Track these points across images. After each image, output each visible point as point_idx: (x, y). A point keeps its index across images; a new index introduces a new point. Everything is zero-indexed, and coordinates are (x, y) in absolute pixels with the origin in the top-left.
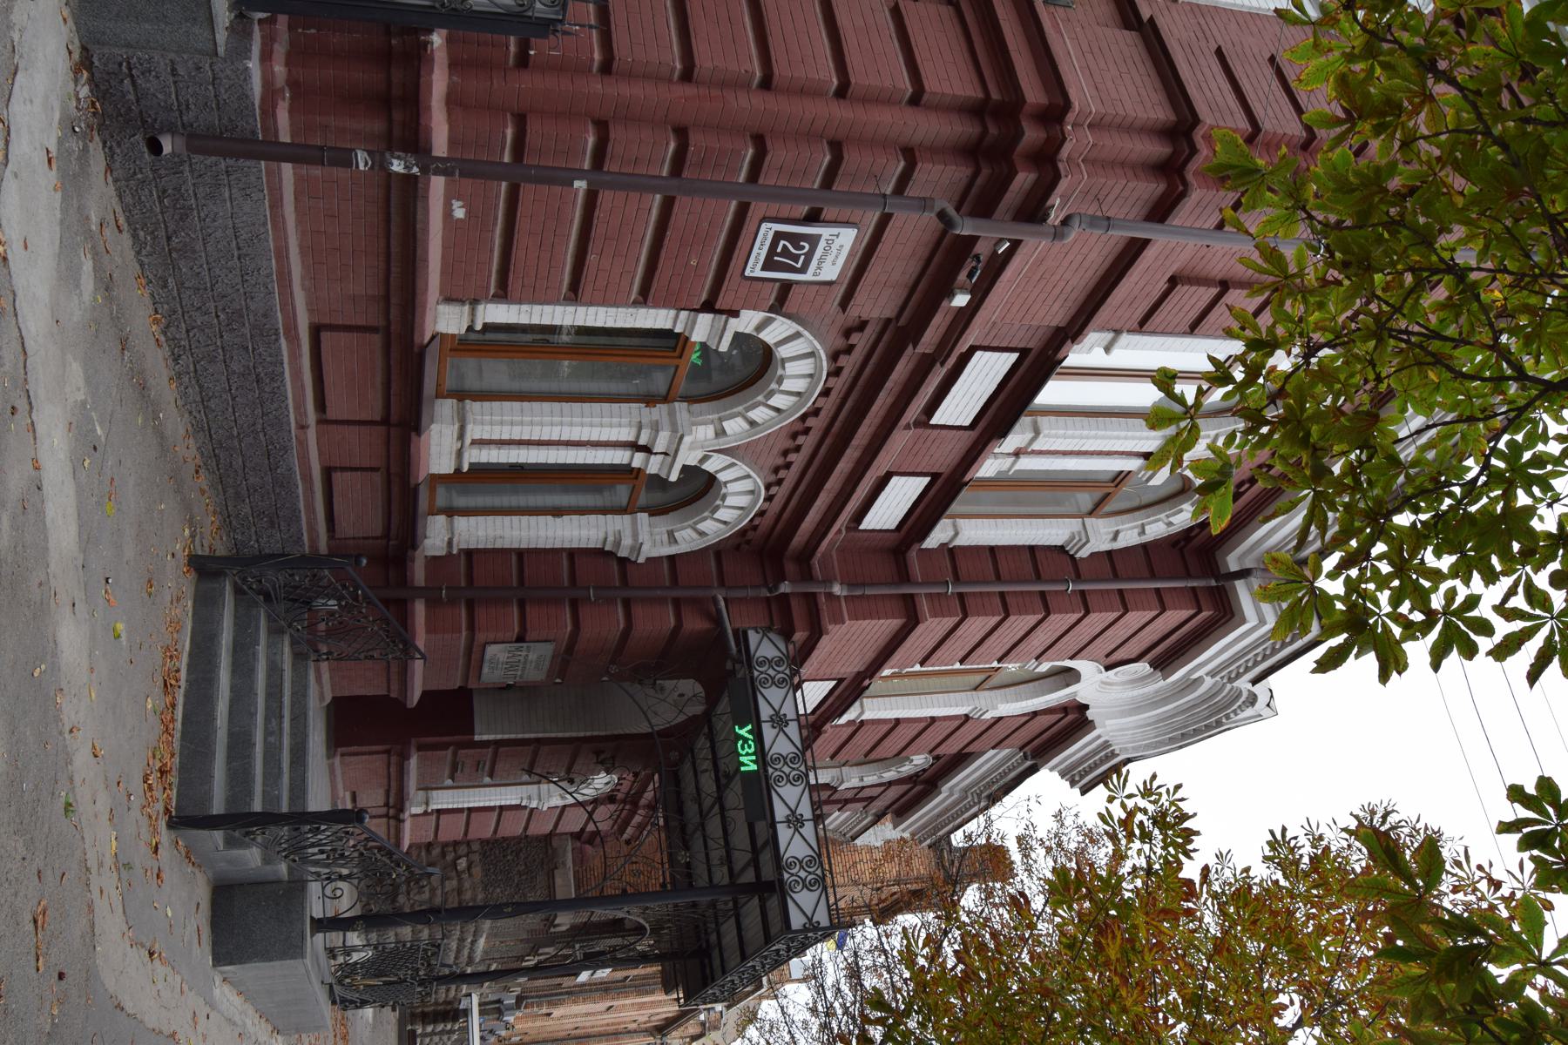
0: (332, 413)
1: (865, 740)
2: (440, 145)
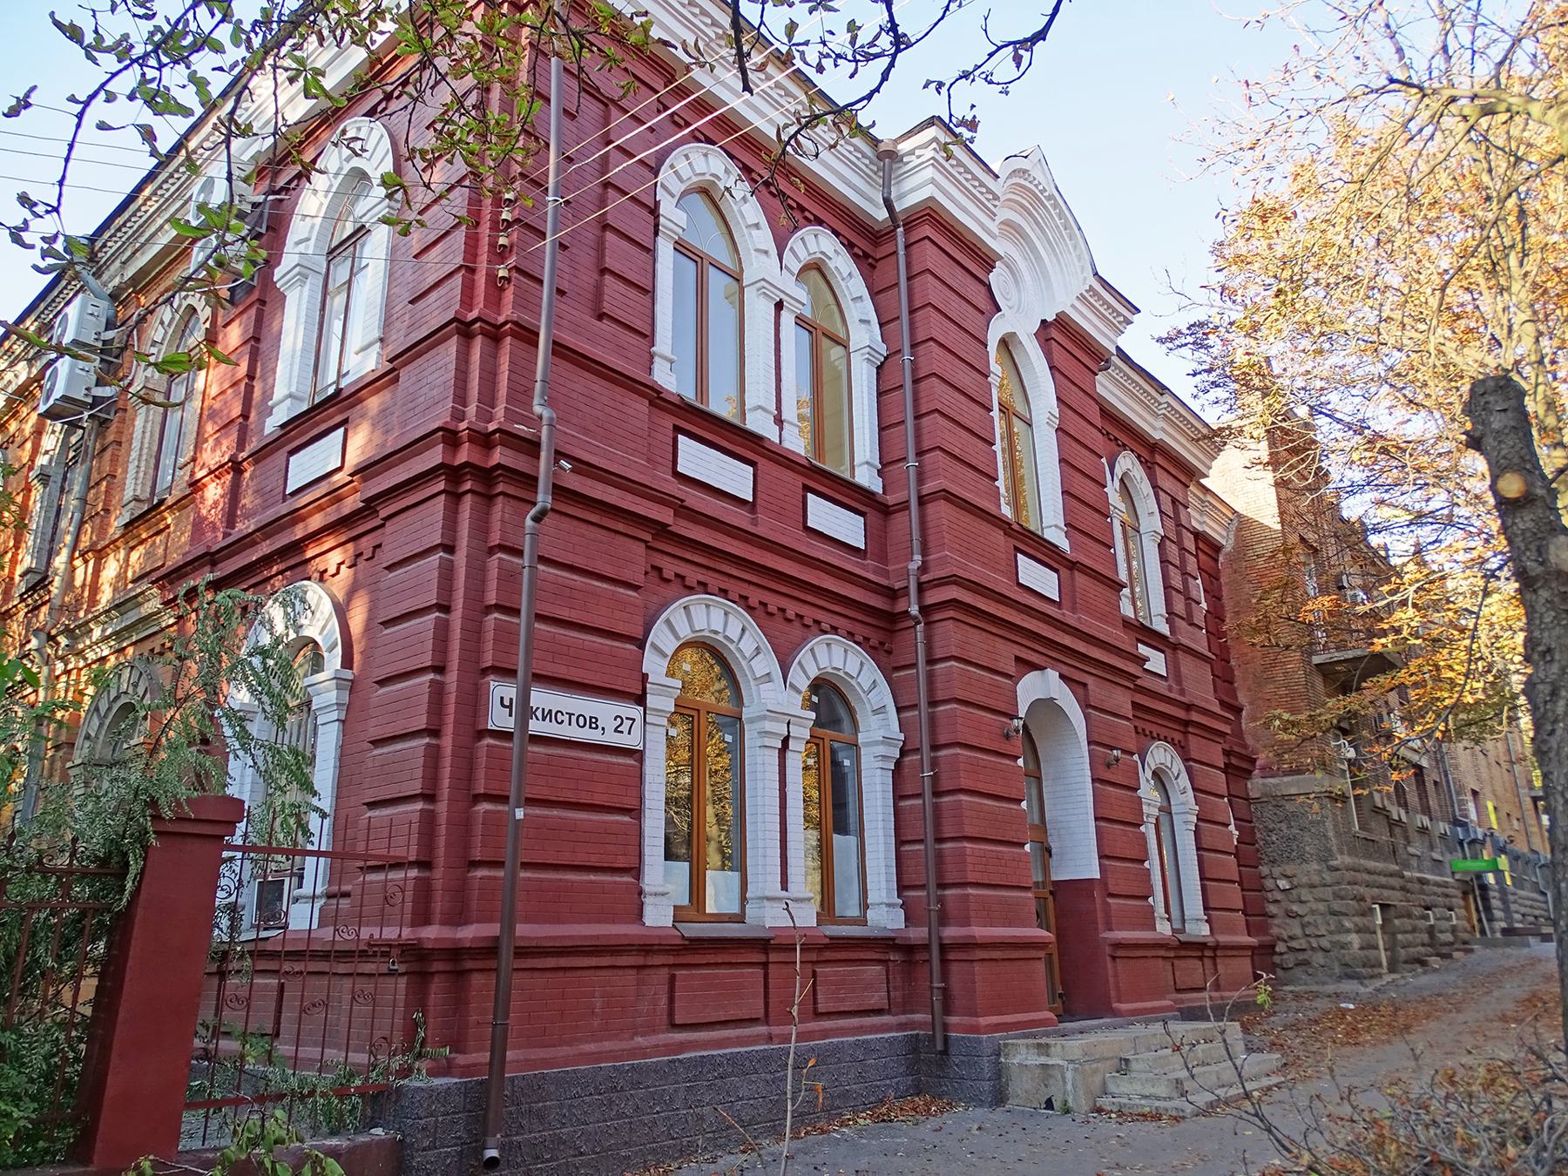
0: (760, 1013)
1: (1088, 520)
2: (493, 929)
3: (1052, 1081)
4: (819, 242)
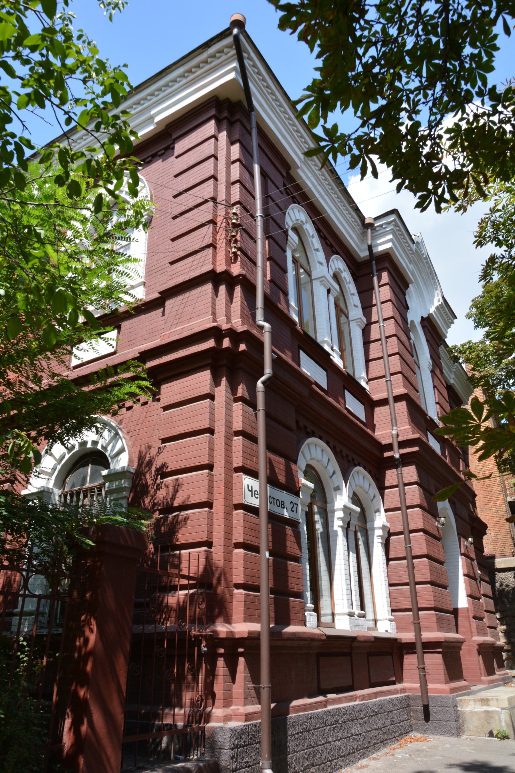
3: (492, 721)
4: (338, 263)
